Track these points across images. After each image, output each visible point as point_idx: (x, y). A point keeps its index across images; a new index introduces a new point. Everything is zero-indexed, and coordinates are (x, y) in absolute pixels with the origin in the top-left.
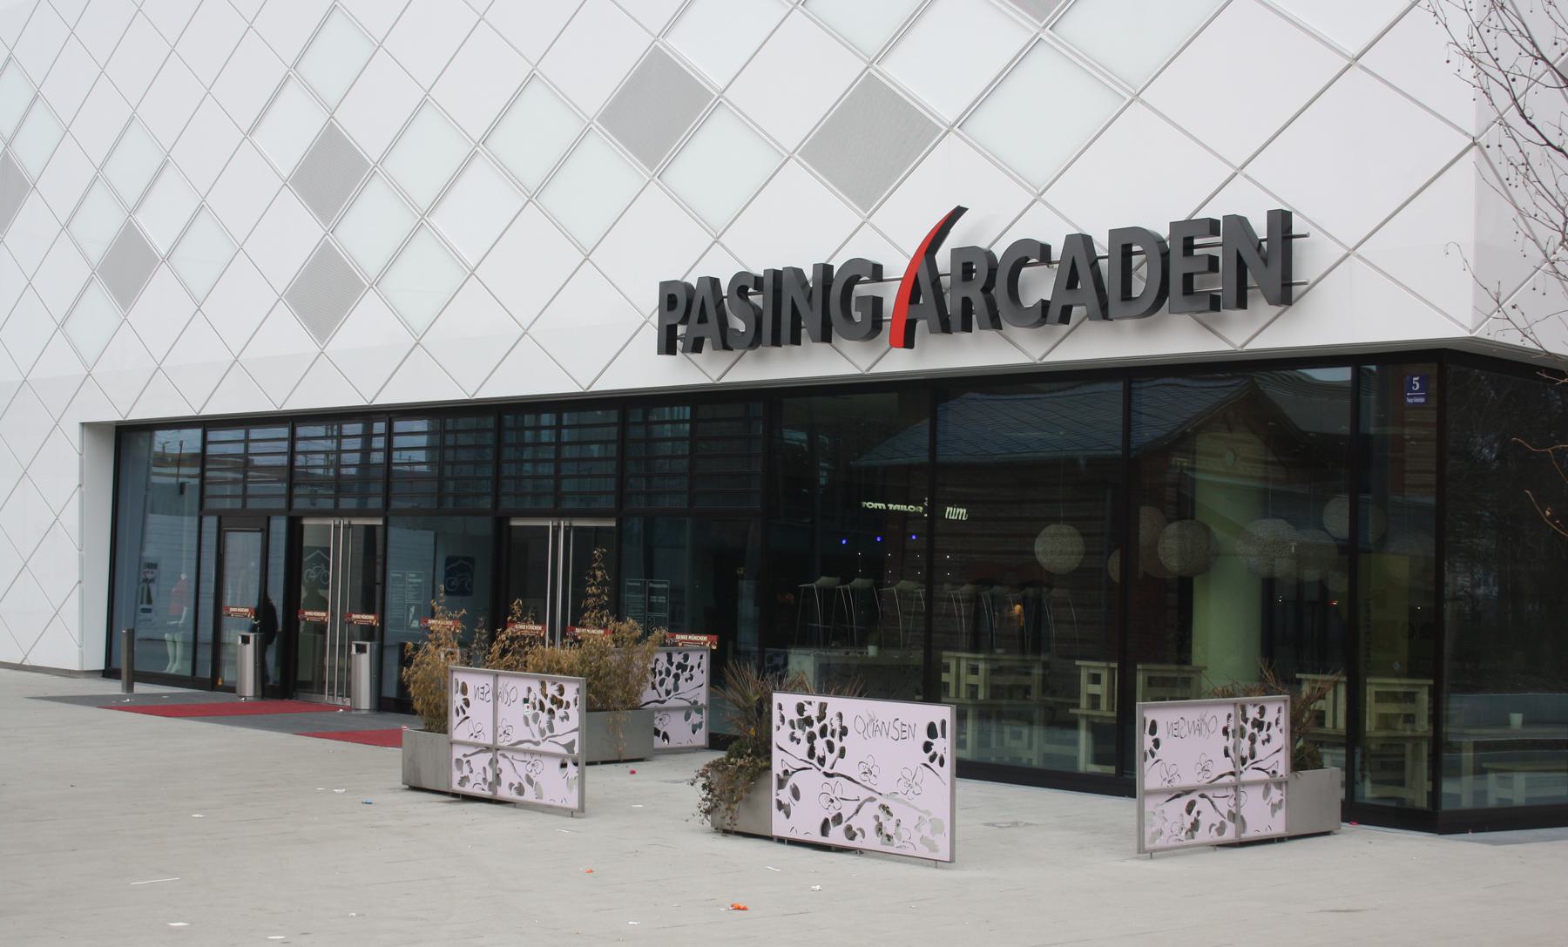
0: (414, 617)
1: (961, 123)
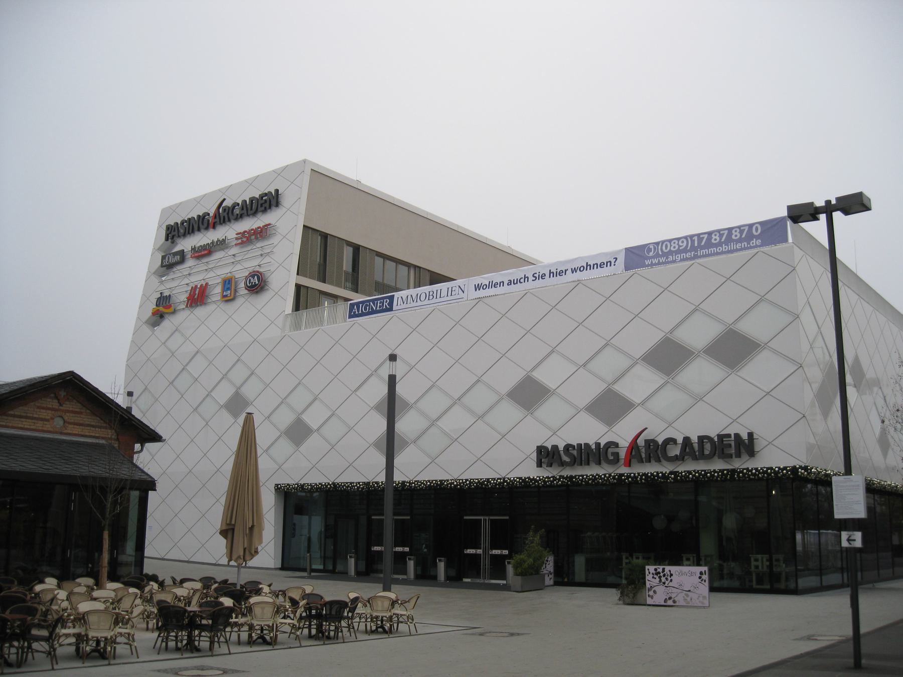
0: (425, 548)
1: (318, 429)
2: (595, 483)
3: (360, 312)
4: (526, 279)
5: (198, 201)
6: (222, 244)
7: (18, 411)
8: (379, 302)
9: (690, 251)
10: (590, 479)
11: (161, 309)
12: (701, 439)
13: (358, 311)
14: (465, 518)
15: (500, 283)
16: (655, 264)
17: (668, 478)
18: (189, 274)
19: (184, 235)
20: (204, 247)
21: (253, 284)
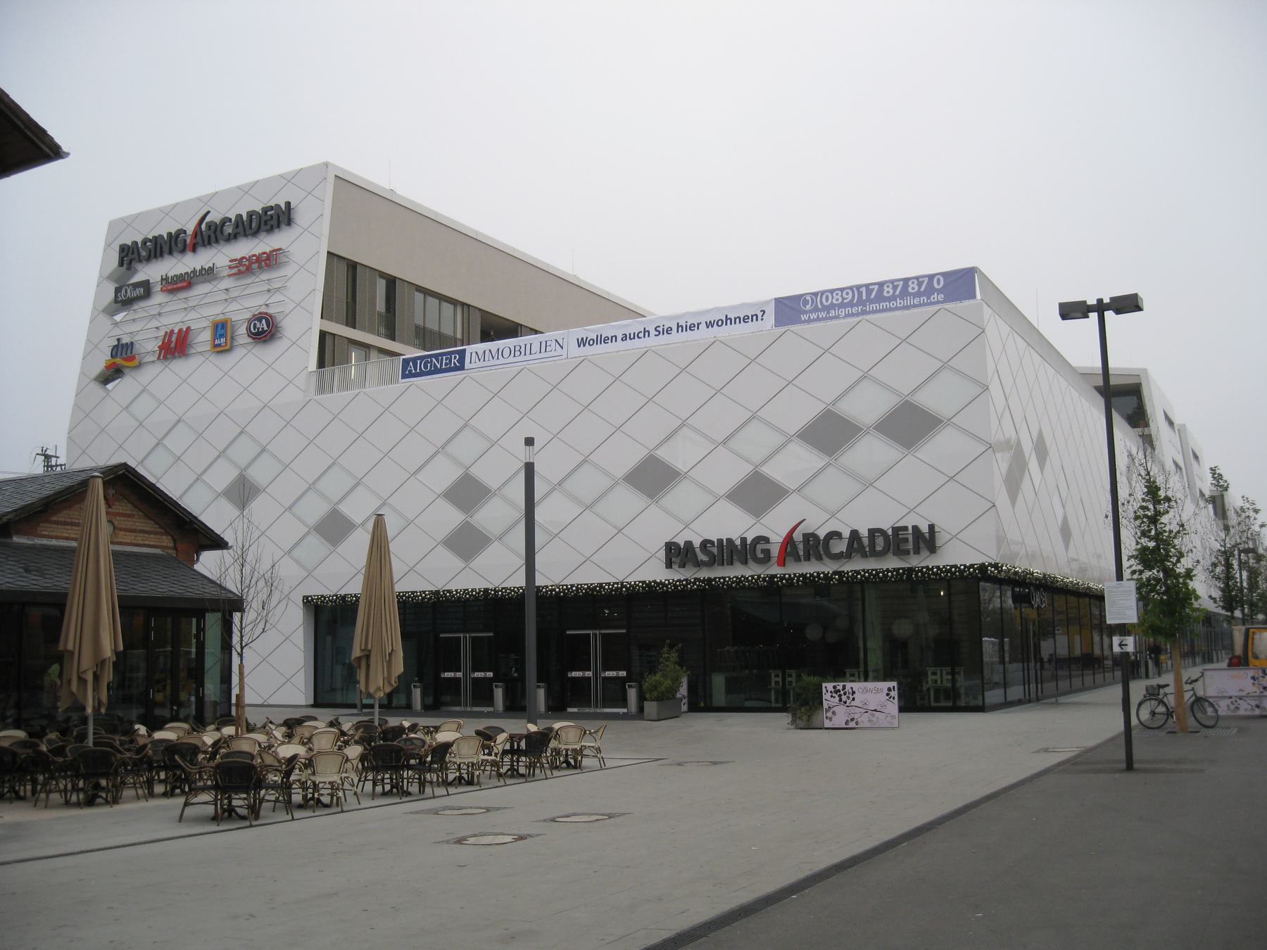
0: (515, 672)
2: (740, 586)
3: (418, 371)
4: (647, 334)
5: (167, 212)
6: (208, 274)
7: (61, 516)
8: (444, 358)
9: (857, 305)
10: (733, 582)
11: (118, 361)
12: (872, 532)
13: (416, 369)
14: (568, 632)
15: (612, 337)
16: (814, 320)
17: (831, 579)
18: (160, 314)
19: (148, 259)
20: (180, 278)
21: (261, 330)
